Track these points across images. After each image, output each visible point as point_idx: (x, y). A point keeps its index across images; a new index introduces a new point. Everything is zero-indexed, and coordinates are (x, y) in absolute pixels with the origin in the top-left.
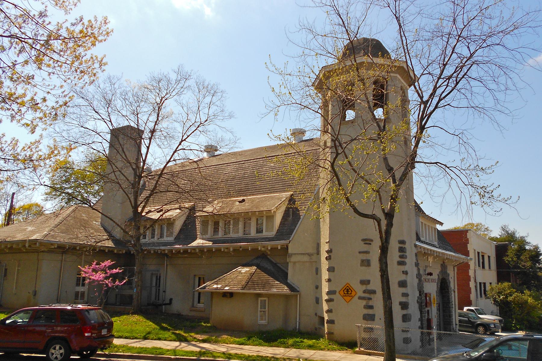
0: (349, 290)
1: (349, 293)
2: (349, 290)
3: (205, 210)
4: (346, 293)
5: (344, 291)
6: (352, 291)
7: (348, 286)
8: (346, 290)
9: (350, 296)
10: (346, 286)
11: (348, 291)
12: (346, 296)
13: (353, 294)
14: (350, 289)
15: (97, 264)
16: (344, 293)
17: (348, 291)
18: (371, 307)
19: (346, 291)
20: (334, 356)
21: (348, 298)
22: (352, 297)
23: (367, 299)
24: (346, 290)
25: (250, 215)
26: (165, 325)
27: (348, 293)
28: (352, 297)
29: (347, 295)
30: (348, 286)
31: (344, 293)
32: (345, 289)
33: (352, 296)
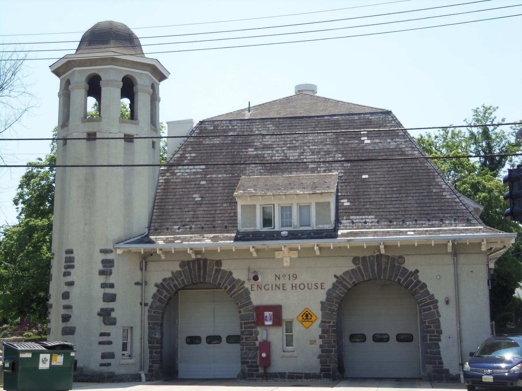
0: (309, 315)
1: (309, 318)
2: (309, 315)
3: (248, 190)
4: (305, 318)
5: (311, 319)
6: (312, 316)
7: (307, 311)
8: (305, 315)
9: (310, 321)
10: (305, 311)
11: (307, 316)
12: (305, 321)
13: (313, 318)
14: (309, 314)
15: (40, 171)
16: (303, 319)
17: (307, 316)
18: (112, 286)
19: (306, 316)
20: (219, 150)
21: (307, 324)
22: (312, 323)
23: (68, 252)
24: (305, 315)
25: (287, 263)
26: (403, 338)
27: (307, 319)
28: (312, 323)
29: (306, 320)
30: (307, 311)
31: (303, 319)
32: (304, 314)
33: (312, 321)
